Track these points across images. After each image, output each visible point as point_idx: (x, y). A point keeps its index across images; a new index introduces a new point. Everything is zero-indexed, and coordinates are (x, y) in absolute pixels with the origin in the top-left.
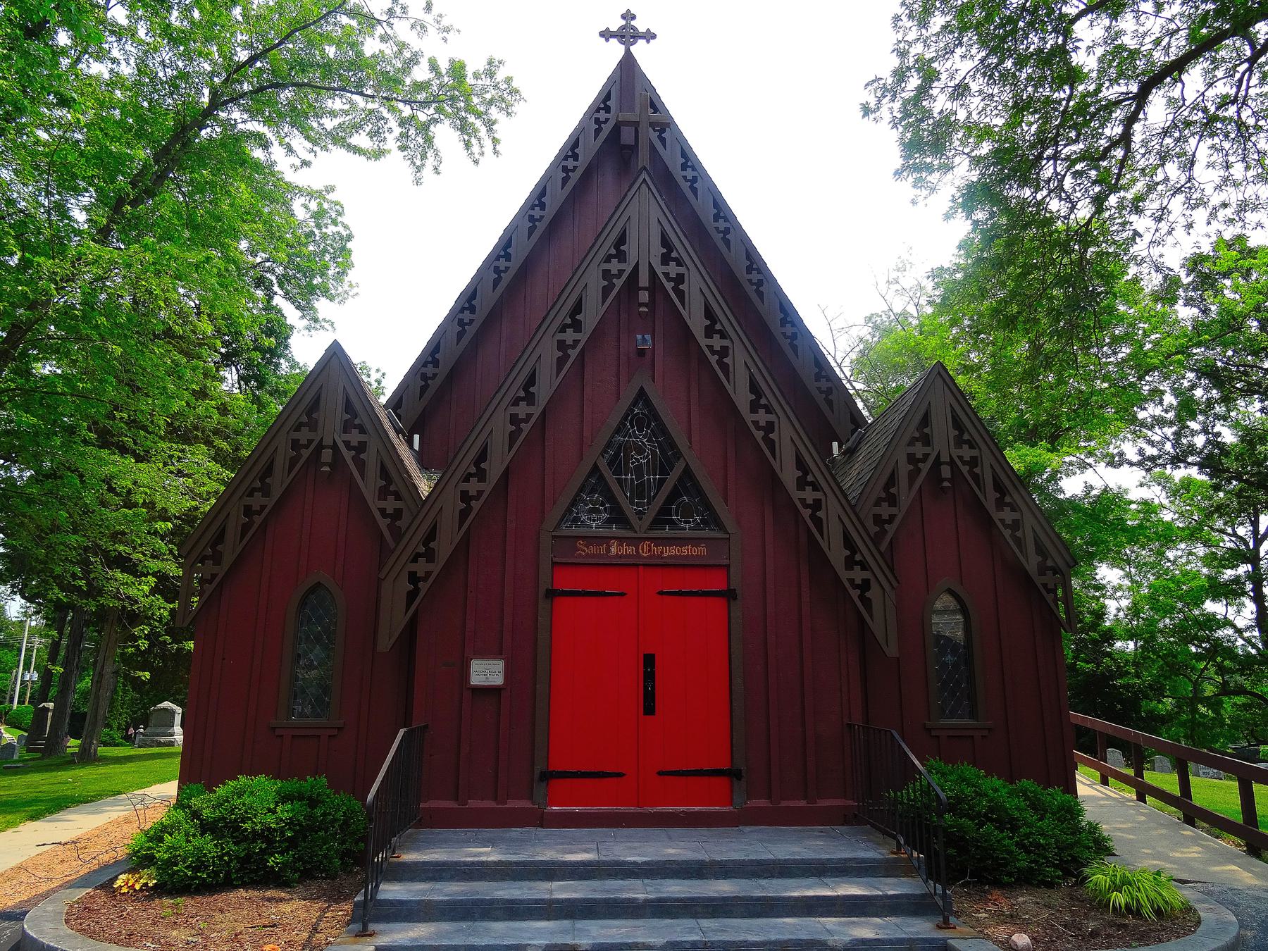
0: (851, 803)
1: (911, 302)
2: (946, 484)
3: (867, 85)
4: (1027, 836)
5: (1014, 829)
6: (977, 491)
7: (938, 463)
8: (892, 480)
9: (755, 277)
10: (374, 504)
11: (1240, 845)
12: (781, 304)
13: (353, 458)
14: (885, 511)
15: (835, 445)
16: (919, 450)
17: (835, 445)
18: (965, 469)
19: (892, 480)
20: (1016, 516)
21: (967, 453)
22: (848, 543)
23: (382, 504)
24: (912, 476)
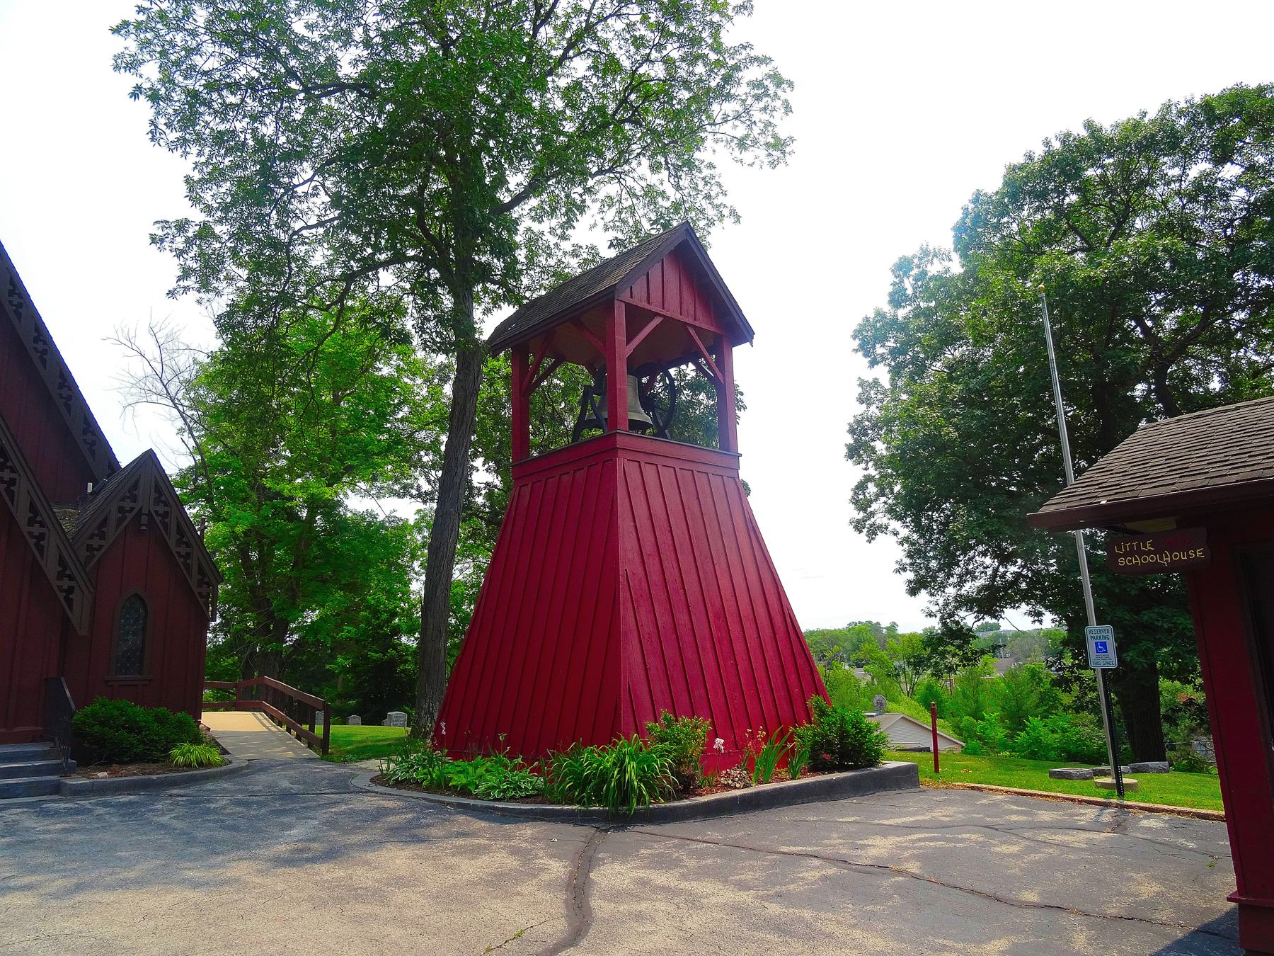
0: (39, 728)
1: (176, 379)
2: (143, 528)
3: (156, 222)
4: (146, 736)
5: (139, 733)
6: (166, 537)
7: (139, 514)
8: (104, 522)
9: (40, 346)
10: (174, 549)
11: (381, 813)
12: (61, 372)
13: (35, 544)
14: (96, 542)
15: (90, 485)
16: (127, 504)
17: (90, 485)
18: (158, 519)
19: (104, 522)
20: (188, 550)
21: (161, 509)
22: (62, 562)
23: (178, 549)
24: (120, 521)
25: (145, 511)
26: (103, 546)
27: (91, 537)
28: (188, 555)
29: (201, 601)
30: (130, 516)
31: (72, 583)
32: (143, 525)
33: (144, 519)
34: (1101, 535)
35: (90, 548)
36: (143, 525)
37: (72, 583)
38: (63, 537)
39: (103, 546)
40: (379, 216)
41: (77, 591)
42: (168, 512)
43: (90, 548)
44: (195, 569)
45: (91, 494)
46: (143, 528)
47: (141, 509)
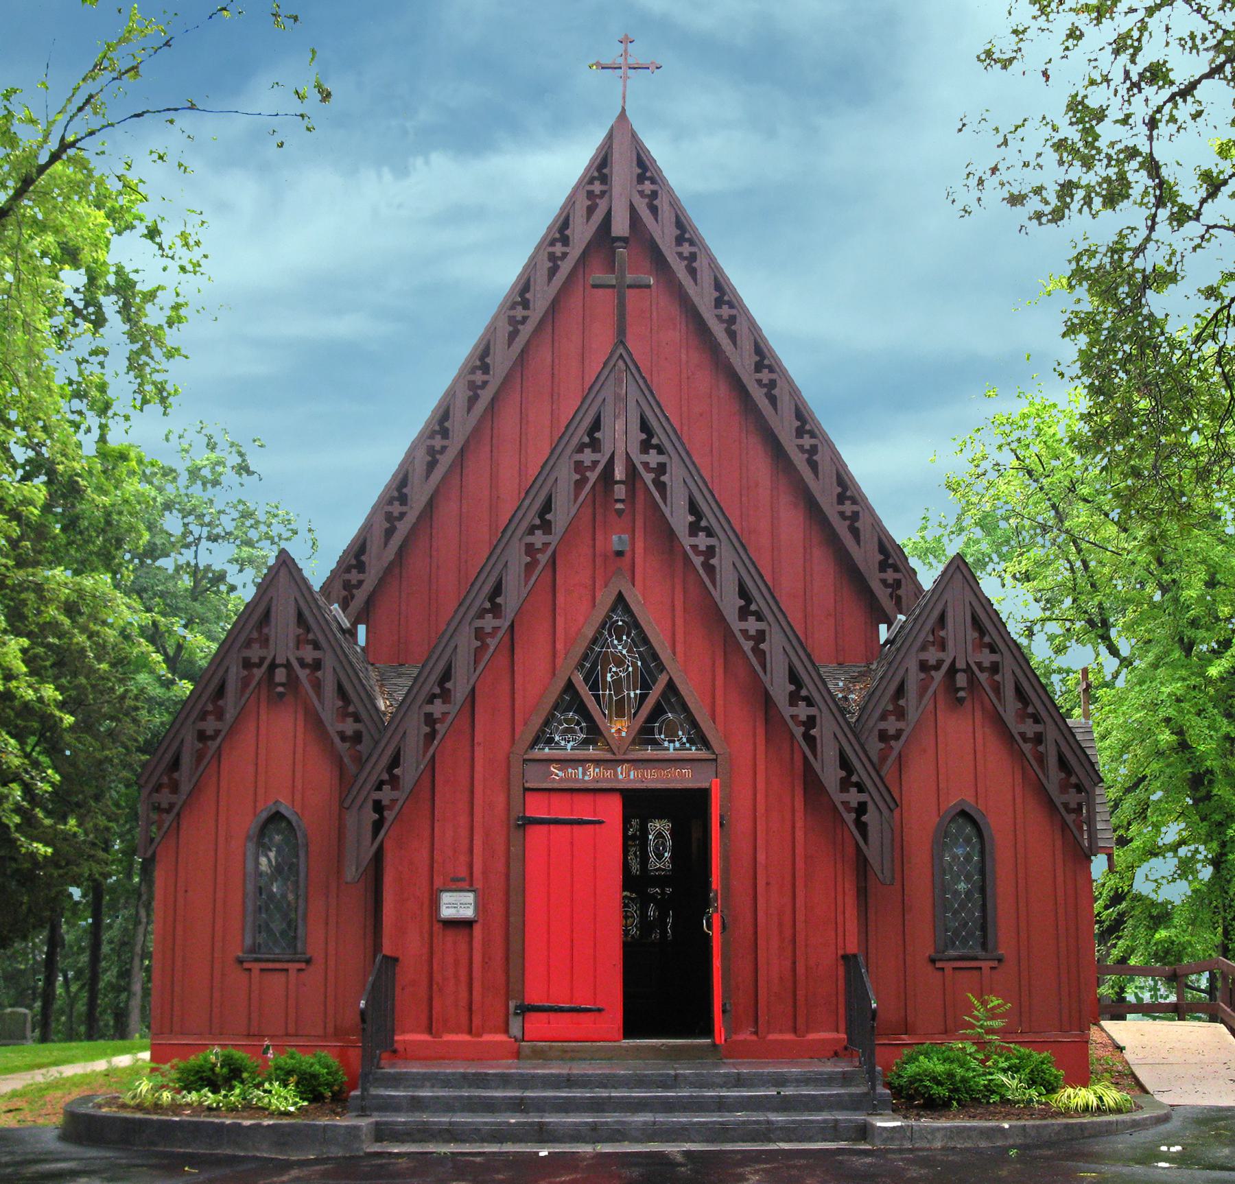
7: (953, 671)
17: (883, 628)
25: (961, 664)
26: (220, 731)
27: (883, 717)
28: (1039, 739)
29: (1070, 818)
30: (593, 476)
31: (863, 797)
32: (618, 501)
33: (961, 680)
34: (624, 734)
35: (883, 736)
36: (618, 501)
37: (863, 797)
38: (421, 680)
39: (220, 731)
40: (963, 906)
41: (871, 807)
42: (997, 663)
43: (883, 736)
44: (1052, 761)
45: (887, 642)
46: (961, 694)
47: (954, 661)
